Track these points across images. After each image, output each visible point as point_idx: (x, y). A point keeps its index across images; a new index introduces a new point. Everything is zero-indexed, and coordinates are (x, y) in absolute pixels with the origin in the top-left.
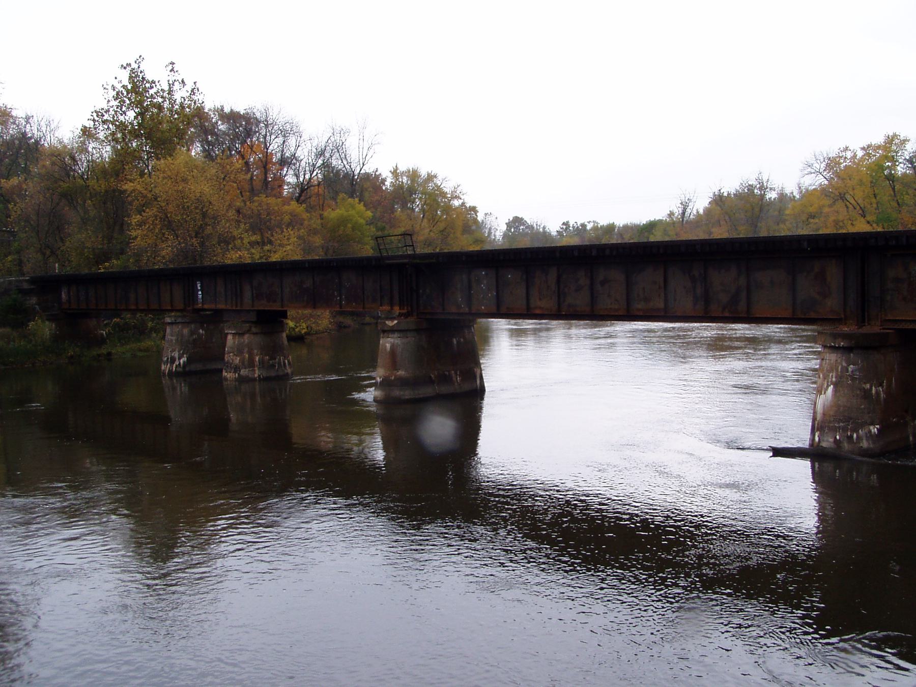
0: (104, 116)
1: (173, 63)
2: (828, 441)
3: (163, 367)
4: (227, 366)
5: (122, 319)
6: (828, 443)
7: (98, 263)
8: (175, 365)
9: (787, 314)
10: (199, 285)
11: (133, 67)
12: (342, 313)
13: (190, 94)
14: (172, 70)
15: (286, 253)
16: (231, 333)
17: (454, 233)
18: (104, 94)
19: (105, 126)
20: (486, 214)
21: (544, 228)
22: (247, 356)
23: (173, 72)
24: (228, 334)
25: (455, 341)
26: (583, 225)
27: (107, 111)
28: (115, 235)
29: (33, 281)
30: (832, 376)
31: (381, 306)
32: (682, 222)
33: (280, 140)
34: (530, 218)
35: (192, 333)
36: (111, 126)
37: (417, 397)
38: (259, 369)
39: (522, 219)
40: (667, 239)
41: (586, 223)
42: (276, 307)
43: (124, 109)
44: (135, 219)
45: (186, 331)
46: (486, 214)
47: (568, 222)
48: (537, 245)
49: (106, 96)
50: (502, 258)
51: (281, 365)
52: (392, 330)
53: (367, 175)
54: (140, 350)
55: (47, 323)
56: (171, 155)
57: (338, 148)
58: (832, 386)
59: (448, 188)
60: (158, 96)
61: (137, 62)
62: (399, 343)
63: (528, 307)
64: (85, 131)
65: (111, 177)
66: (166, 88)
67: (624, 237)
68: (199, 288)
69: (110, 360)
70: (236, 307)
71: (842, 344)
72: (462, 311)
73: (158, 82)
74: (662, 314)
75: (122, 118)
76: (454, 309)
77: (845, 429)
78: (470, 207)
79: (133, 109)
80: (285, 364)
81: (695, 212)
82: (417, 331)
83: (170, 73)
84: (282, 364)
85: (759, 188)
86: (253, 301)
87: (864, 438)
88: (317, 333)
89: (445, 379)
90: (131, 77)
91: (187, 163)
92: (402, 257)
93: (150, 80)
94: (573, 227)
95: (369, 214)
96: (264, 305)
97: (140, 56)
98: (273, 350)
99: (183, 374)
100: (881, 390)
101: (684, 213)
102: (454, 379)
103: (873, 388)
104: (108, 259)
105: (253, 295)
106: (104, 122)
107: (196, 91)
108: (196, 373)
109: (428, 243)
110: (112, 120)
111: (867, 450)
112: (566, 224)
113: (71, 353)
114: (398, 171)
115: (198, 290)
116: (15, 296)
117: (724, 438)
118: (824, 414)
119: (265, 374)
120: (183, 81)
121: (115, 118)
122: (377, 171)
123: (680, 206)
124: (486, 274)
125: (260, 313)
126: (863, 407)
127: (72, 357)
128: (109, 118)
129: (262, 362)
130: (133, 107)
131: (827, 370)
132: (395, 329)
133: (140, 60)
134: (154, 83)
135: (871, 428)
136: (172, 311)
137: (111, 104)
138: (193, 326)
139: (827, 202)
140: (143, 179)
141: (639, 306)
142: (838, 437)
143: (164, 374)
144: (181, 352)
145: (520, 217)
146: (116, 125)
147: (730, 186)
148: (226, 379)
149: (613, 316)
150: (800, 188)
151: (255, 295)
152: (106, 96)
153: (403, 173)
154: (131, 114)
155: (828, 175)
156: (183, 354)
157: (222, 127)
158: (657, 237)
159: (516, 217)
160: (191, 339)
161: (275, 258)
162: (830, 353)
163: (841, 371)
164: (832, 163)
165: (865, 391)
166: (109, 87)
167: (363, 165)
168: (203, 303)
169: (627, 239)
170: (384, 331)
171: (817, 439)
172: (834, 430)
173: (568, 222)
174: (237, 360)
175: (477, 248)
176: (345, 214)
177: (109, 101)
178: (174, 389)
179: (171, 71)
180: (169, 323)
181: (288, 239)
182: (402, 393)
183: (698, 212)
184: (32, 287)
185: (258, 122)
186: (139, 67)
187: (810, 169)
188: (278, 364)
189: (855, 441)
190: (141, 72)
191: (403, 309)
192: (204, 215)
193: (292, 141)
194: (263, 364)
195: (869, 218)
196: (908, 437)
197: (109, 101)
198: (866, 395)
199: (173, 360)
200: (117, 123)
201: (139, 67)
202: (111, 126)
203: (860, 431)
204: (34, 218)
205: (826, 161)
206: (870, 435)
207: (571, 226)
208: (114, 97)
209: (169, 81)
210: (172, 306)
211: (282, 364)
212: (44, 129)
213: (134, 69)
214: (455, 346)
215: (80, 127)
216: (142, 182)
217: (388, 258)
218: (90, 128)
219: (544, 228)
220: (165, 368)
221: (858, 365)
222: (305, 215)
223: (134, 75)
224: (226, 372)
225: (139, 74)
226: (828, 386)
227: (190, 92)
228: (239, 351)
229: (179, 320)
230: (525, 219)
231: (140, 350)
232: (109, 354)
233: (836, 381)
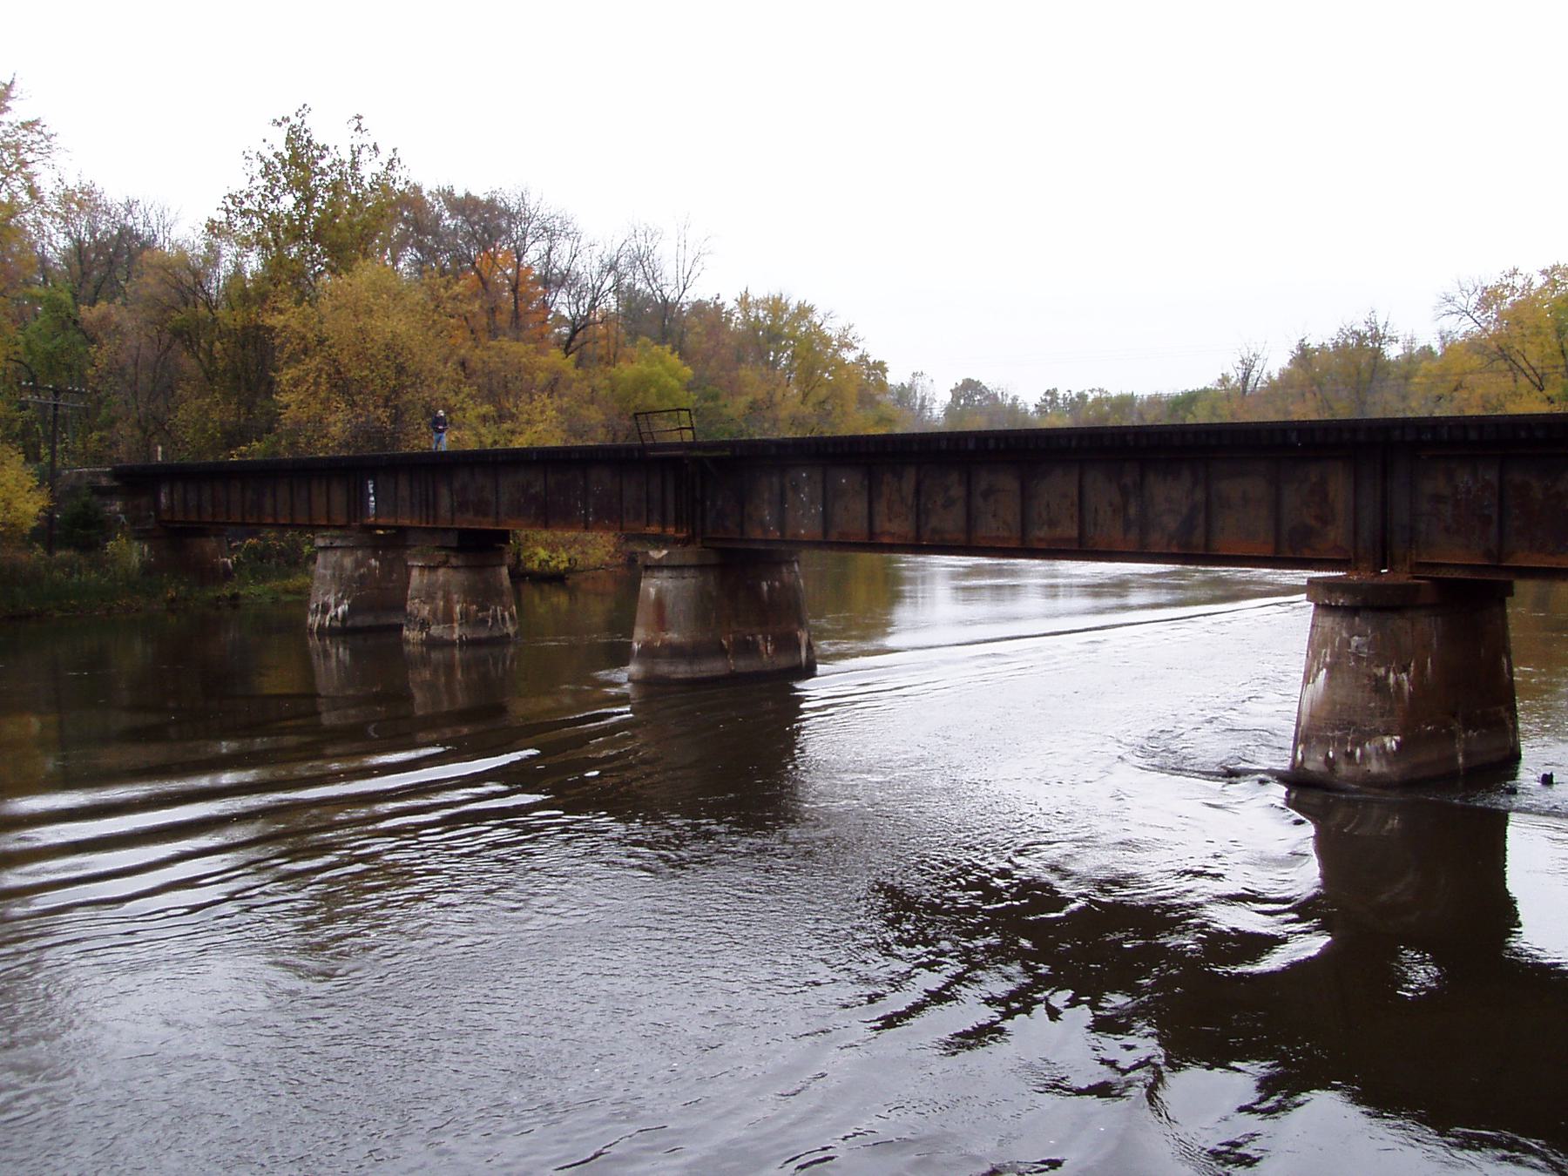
0: (243, 203)
1: (359, 117)
2: (1315, 760)
3: (310, 620)
4: (410, 621)
5: (260, 539)
6: (1315, 764)
7: (230, 446)
8: (328, 617)
9: (1267, 551)
10: (371, 486)
11: (293, 122)
12: (628, 539)
13: (387, 168)
14: (358, 128)
15: (536, 435)
17: (842, 406)
18: (246, 167)
19: (245, 219)
20: (914, 374)
21: (1015, 399)
22: (442, 603)
23: (359, 132)
24: (413, 566)
25: (765, 586)
26: (1082, 396)
27: (249, 196)
28: (258, 400)
29: (118, 474)
30: (1326, 653)
31: (648, 526)
32: (1240, 392)
33: (543, 245)
34: (991, 380)
35: (358, 564)
36: (254, 220)
37: (697, 676)
38: (461, 625)
39: (978, 383)
40: (1216, 420)
41: (1086, 393)
42: (487, 524)
43: (277, 192)
44: (286, 375)
45: (348, 562)
46: (914, 374)
47: (1055, 390)
48: (1005, 426)
49: (248, 169)
50: (830, 450)
52: (659, 566)
53: (699, 307)
54: (287, 592)
55: (136, 544)
56: (348, 270)
57: (638, 260)
58: (1325, 670)
59: (832, 329)
60: (332, 171)
61: (300, 114)
62: (671, 587)
63: (872, 534)
64: (212, 227)
65: (255, 304)
66: (348, 158)
67: (1146, 417)
68: (371, 491)
69: (236, 607)
71: (1341, 601)
73: (336, 147)
74: (1075, 547)
75: (272, 207)
76: (757, 534)
77: (1342, 742)
78: (874, 362)
79: (291, 192)
80: (503, 618)
81: (1264, 377)
82: (700, 567)
83: (354, 134)
84: (499, 617)
85: (1371, 337)
86: (453, 514)
87: (1374, 756)
88: (586, 570)
89: (747, 648)
90: (289, 140)
91: (374, 283)
92: (679, 446)
93: (321, 145)
94: (1065, 399)
95: (688, 371)
96: (468, 521)
97: (304, 106)
98: (483, 595)
99: (342, 632)
100: (1405, 678)
101: (1246, 378)
102: (762, 648)
103: (1392, 675)
104: (245, 440)
105: (452, 505)
106: (244, 213)
107: (396, 163)
108: (369, 630)
109: (795, 421)
110: (257, 209)
111: (1380, 775)
112: (1052, 393)
113: (172, 593)
114: (750, 299)
115: (370, 495)
116: (87, 498)
118: (1311, 716)
119: (469, 634)
120: (375, 148)
121: (263, 207)
122: (718, 298)
123: (1240, 366)
124: (809, 477)
125: (464, 534)
126: (1372, 705)
127: (173, 600)
128: (252, 207)
129: (465, 614)
130: (292, 189)
131: (1318, 646)
132: (664, 563)
133: (303, 112)
134: (327, 149)
135: (1387, 739)
136: (327, 527)
137: (255, 184)
138: (360, 554)
139: (1476, 361)
140: (301, 309)
141: (1041, 533)
142: (1331, 754)
143: (311, 630)
144: (340, 595)
145: (976, 380)
146: (263, 219)
147: (1323, 333)
148: (408, 642)
149: (1001, 548)
150: (1442, 338)
152: (248, 169)
153: (757, 304)
154: (288, 202)
155: (1483, 317)
156: (343, 598)
157: (448, 222)
158: (1200, 416)
159: (969, 380)
160: (357, 574)
161: (519, 442)
162: (1323, 616)
163: (1339, 646)
164: (1489, 298)
165: (1377, 679)
166: (253, 155)
167: (685, 289)
168: (376, 516)
169: (1149, 420)
170: (647, 568)
171: (1299, 756)
172: (1325, 742)
173: (1055, 390)
174: (425, 611)
175: (882, 431)
176: (646, 370)
177: (252, 179)
178: (327, 655)
179: (356, 130)
181: (542, 412)
182: (672, 668)
183: (1269, 377)
184: (115, 484)
185: (512, 217)
186: (303, 123)
187: (1449, 307)
189: (1358, 760)
190: (306, 131)
191: (682, 532)
192: (401, 370)
193: (563, 248)
195: (1549, 392)
196: (1455, 758)
197: (252, 179)
198: (1379, 686)
199: (326, 609)
200: (266, 216)
201: (303, 123)
202: (254, 220)
203: (1367, 745)
204: (131, 370)
205: (1479, 292)
206: (1383, 752)
207: (1061, 396)
208: (261, 171)
209: (352, 146)
210: (329, 519)
211: (499, 617)
212: (154, 223)
213: (295, 127)
214: (765, 595)
215: (205, 221)
216: (299, 314)
217: (656, 447)
218: (221, 223)
219: (1015, 399)
220: (313, 620)
221: (1367, 636)
222: (573, 373)
223: (293, 136)
224: (409, 630)
225: (302, 134)
226: (1319, 670)
227: (385, 165)
228: (429, 597)
229: (337, 543)
230: (984, 384)
231: (287, 592)
232: (235, 597)
233: (1331, 663)
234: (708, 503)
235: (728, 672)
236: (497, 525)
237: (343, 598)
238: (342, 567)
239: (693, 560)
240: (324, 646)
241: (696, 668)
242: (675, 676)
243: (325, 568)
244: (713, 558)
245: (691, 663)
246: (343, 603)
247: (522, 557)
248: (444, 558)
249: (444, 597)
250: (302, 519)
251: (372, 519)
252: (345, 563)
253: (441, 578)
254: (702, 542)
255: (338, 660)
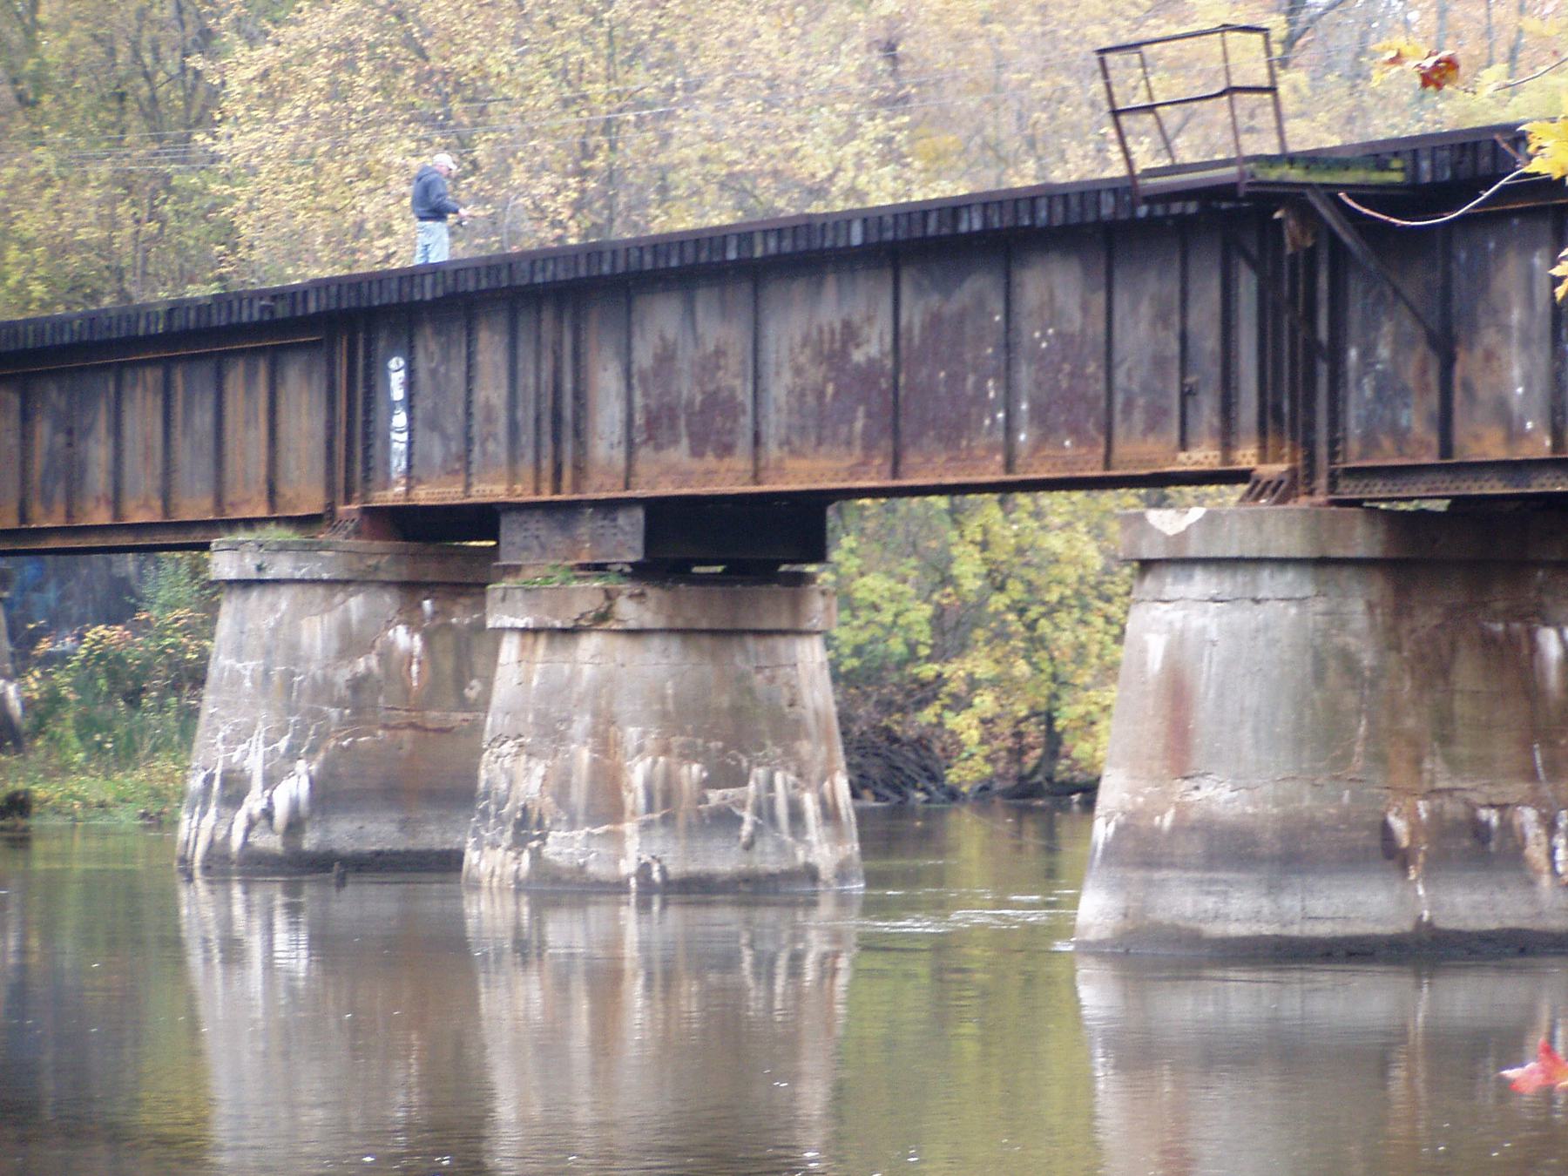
3: (183, 832)
16: (513, 629)
24: (503, 630)
35: (350, 643)
37: (1294, 931)
38: (646, 826)
51: (773, 820)
62: (1213, 633)
70: (557, 490)
72: (1526, 452)
80: (796, 815)
115: (392, 406)
117: (989, 537)
119: (676, 859)
129: (663, 797)
132: (1192, 552)
138: (356, 604)
143: (185, 861)
144: (283, 744)
151: (639, 419)
156: (292, 754)
160: (343, 675)
178: (233, 951)
180: (230, 583)
182: (1209, 903)
188: (758, 812)
191: (1278, 459)
194: (667, 802)
199: (233, 790)
224: (478, 846)
228: (551, 733)
229: (282, 567)
234: (1353, 354)
235: (1407, 926)
236: (758, 483)
237: (292, 754)
238: (293, 653)
239: (1292, 543)
240: (227, 922)
241: (1291, 903)
242: (1215, 930)
243: (239, 652)
244: (1361, 540)
245: (1274, 889)
246: (288, 773)
247: (1060, 724)
248: (599, 602)
249: (594, 733)
250: (195, 506)
251: (400, 489)
252: (305, 638)
253: (587, 671)
254: (1333, 485)
255: (269, 965)
